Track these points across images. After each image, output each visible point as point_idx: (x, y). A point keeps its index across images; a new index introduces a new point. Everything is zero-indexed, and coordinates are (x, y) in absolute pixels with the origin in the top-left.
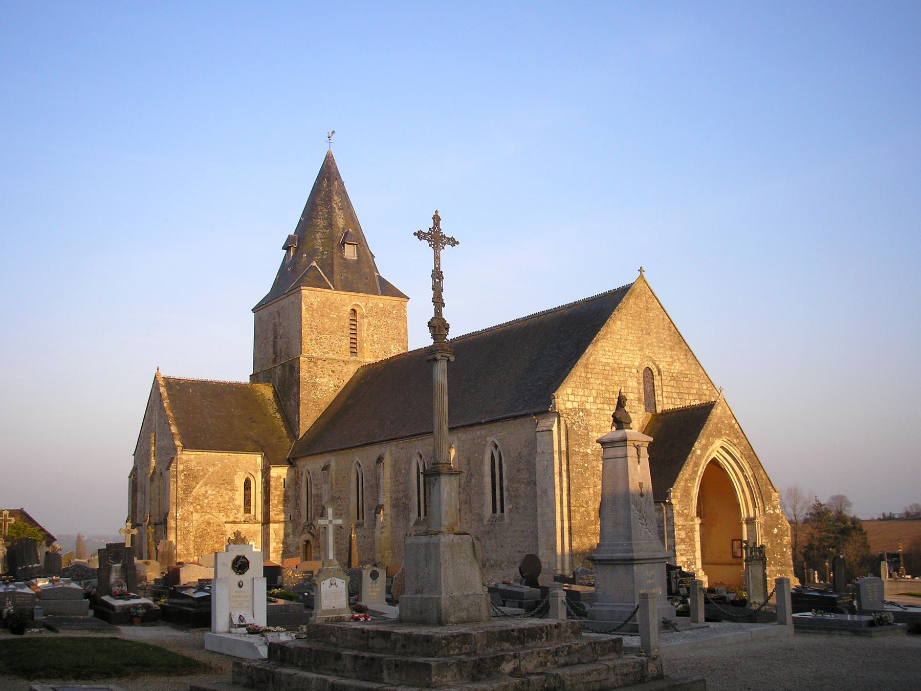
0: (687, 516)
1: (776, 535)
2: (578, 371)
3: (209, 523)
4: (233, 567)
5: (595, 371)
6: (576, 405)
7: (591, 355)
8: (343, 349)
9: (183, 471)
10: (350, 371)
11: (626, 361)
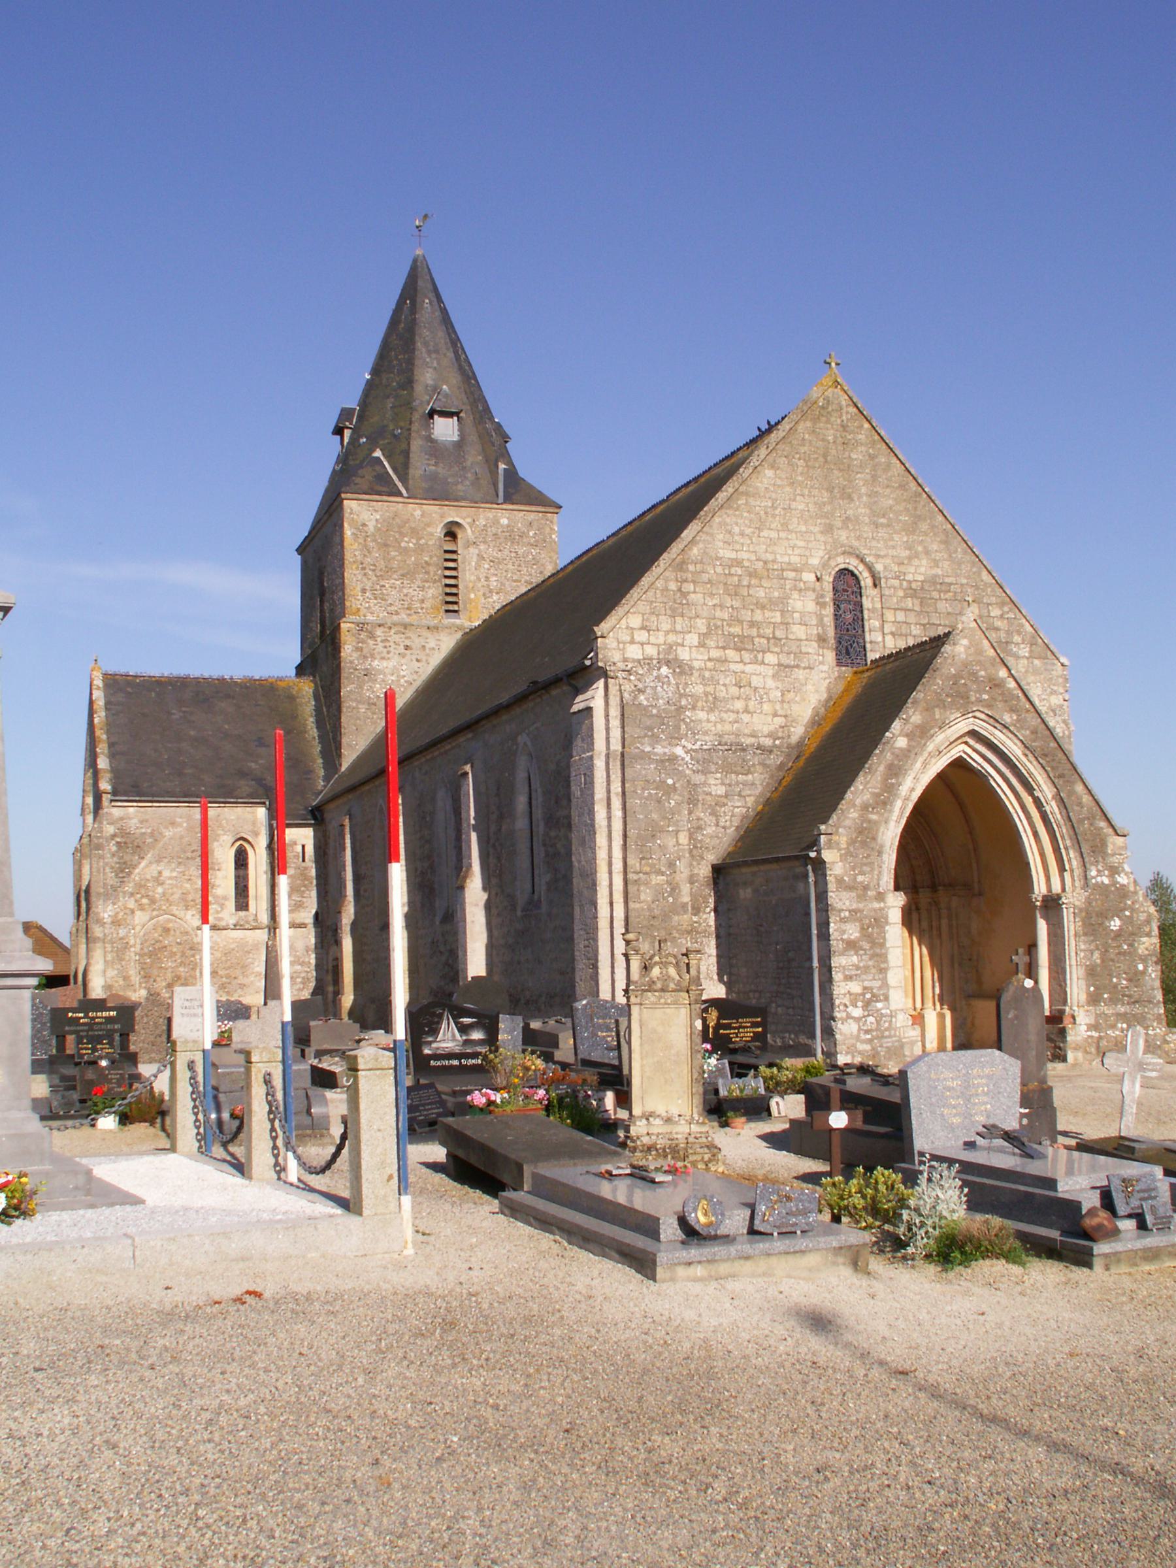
0: (866, 888)
1: (1118, 934)
3: (167, 930)
5: (705, 577)
6: (651, 651)
7: (693, 542)
8: (427, 605)
9: (114, 836)
10: (442, 645)
11: (785, 555)
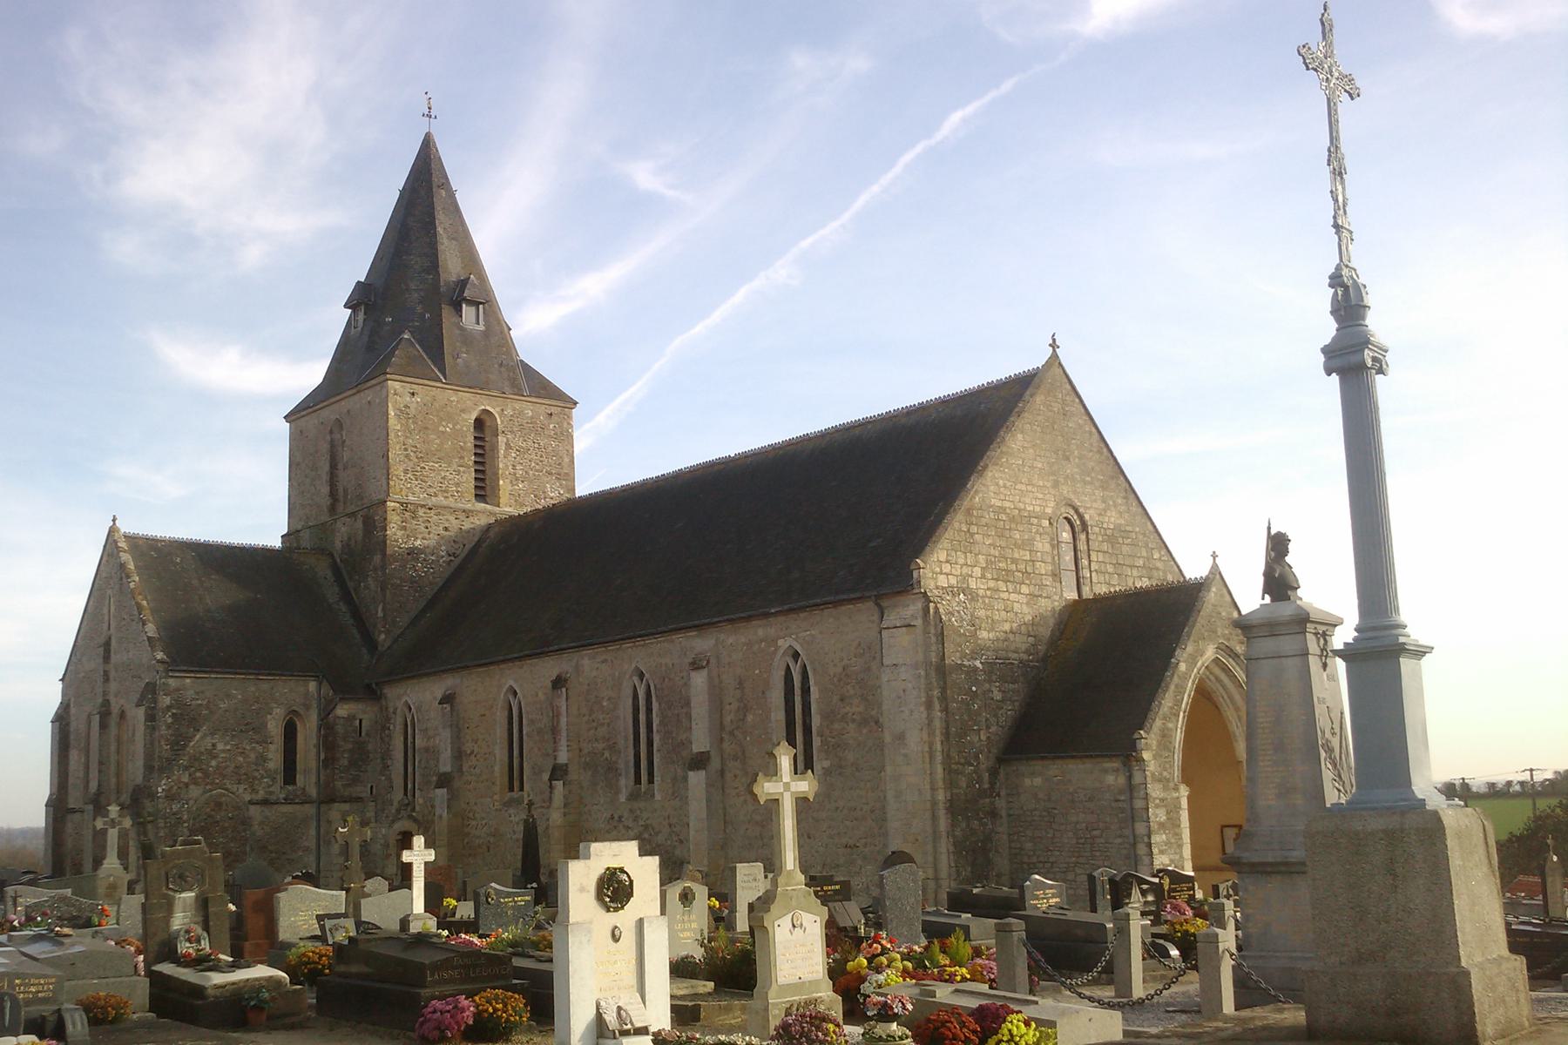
0: (1168, 780)
2: (956, 524)
3: (219, 805)
4: (600, 896)
5: (984, 521)
6: (953, 581)
9: (169, 708)
